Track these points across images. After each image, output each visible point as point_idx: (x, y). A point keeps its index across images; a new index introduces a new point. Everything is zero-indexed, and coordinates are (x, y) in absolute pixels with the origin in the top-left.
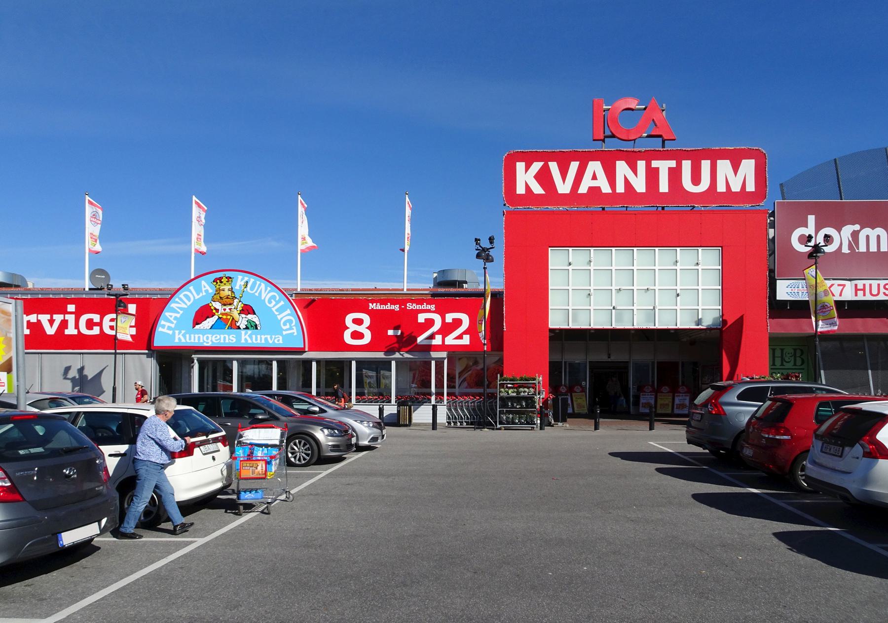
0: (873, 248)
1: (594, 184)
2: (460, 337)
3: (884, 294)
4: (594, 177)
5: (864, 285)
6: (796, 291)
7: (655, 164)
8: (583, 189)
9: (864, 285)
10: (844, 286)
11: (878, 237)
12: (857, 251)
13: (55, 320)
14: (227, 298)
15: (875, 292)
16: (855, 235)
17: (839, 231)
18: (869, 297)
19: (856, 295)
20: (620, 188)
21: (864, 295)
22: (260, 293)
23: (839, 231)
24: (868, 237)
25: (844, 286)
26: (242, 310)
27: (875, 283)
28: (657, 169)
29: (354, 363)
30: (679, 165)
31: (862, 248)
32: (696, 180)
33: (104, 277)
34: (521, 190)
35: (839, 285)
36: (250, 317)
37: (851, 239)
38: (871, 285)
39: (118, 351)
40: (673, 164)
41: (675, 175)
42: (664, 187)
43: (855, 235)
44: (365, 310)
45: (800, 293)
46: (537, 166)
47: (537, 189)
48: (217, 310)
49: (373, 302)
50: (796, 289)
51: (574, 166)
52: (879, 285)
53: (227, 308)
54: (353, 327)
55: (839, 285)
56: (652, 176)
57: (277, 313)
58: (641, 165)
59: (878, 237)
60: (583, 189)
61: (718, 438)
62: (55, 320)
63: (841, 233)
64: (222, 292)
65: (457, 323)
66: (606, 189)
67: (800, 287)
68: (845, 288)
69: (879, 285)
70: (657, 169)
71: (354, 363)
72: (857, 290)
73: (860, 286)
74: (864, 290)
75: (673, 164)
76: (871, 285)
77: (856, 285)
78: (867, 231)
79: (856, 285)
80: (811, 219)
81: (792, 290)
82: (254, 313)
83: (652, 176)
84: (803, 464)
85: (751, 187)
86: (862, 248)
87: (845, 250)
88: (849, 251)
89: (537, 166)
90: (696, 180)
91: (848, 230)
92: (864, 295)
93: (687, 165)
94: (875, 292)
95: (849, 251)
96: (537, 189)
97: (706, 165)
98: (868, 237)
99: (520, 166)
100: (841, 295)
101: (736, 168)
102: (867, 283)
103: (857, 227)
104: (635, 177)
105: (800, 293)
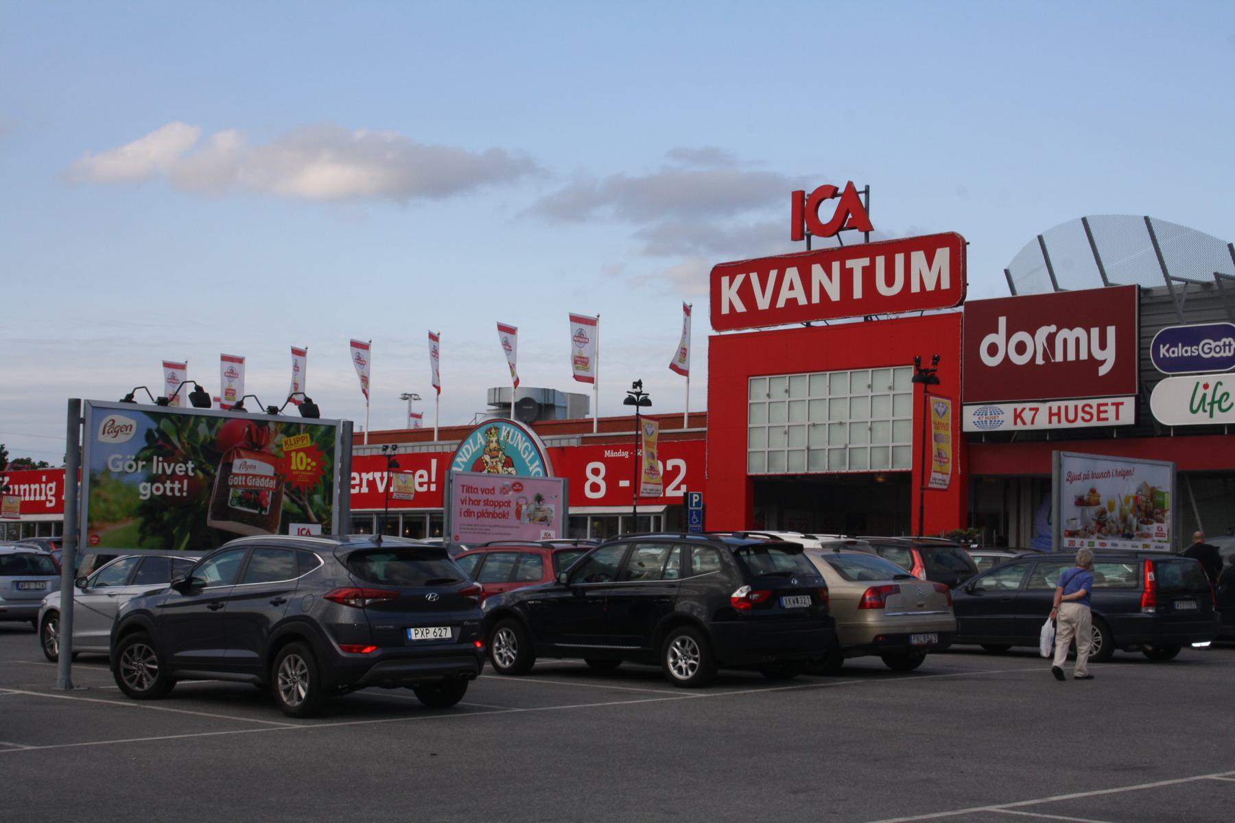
0: (1071, 357)
1: (791, 295)
2: (678, 488)
3: (1083, 418)
4: (791, 288)
5: (1059, 408)
6: (984, 420)
7: (850, 264)
8: (781, 303)
9: (1059, 408)
10: (1037, 410)
11: (1077, 340)
12: (1053, 361)
13: (1216, 275)
14: (495, 450)
15: (1071, 417)
16: (1051, 338)
17: (1033, 335)
18: (1064, 425)
19: (1050, 422)
20: (816, 299)
21: (1059, 421)
22: (518, 444)
23: (1033, 335)
24: (1065, 341)
25: (1037, 410)
26: (505, 463)
27: (1071, 404)
28: (851, 270)
29: (589, 518)
30: (873, 263)
31: (1059, 358)
32: (890, 281)
33: (531, 407)
34: (725, 310)
35: (1031, 409)
36: (510, 469)
37: (1046, 345)
38: (1067, 408)
39: (384, 516)
40: (866, 262)
41: (869, 273)
42: (858, 293)
43: (1051, 338)
44: (601, 458)
45: (988, 422)
46: (740, 279)
47: (740, 308)
48: (487, 463)
49: (608, 448)
50: (984, 416)
51: (773, 274)
52: (1076, 407)
53: (494, 460)
54: (592, 478)
55: (1031, 409)
56: (847, 275)
57: (529, 465)
58: (836, 266)
59: (1077, 340)
60: (781, 303)
61: (846, 623)
62: (1216, 275)
63: (1036, 337)
64: (491, 444)
65: (676, 469)
66: (802, 301)
67: (988, 414)
68: (1038, 413)
69: (1076, 407)
70: (851, 270)
71: (589, 518)
72: (1051, 415)
73: (1055, 410)
74: (1058, 414)
75: (866, 262)
76: (1067, 408)
77: (1050, 408)
78: (1065, 333)
79: (1050, 408)
80: (1002, 321)
81: (979, 418)
82: (513, 466)
83: (847, 275)
84: (1127, 580)
85: (946, 284)
86: (1059, 358)
87: (1040, 361)
88: (1044, 362)
89: (740, 279)
90: (890, 281)
91: (1043, 332)
92: (1059, 421)
93: (880, 261)
94: (1071, 417)
95: (1044, 362)
96: (740, 308)
97: (899, 259)
98: (1065, 341)
99: (725, 280)
100: (1033, 423)
101: (930, 262)
102: (1063, 404)
103: (1053, 328)
104: (732, 300)
105: (988, 422)
